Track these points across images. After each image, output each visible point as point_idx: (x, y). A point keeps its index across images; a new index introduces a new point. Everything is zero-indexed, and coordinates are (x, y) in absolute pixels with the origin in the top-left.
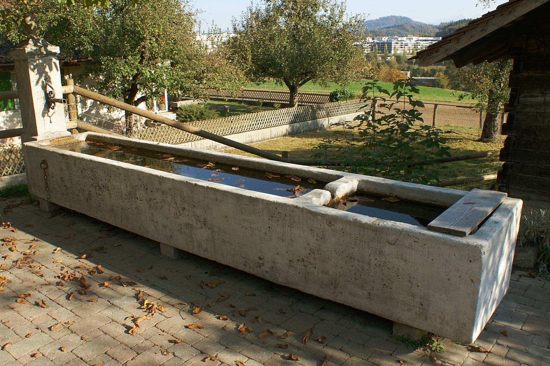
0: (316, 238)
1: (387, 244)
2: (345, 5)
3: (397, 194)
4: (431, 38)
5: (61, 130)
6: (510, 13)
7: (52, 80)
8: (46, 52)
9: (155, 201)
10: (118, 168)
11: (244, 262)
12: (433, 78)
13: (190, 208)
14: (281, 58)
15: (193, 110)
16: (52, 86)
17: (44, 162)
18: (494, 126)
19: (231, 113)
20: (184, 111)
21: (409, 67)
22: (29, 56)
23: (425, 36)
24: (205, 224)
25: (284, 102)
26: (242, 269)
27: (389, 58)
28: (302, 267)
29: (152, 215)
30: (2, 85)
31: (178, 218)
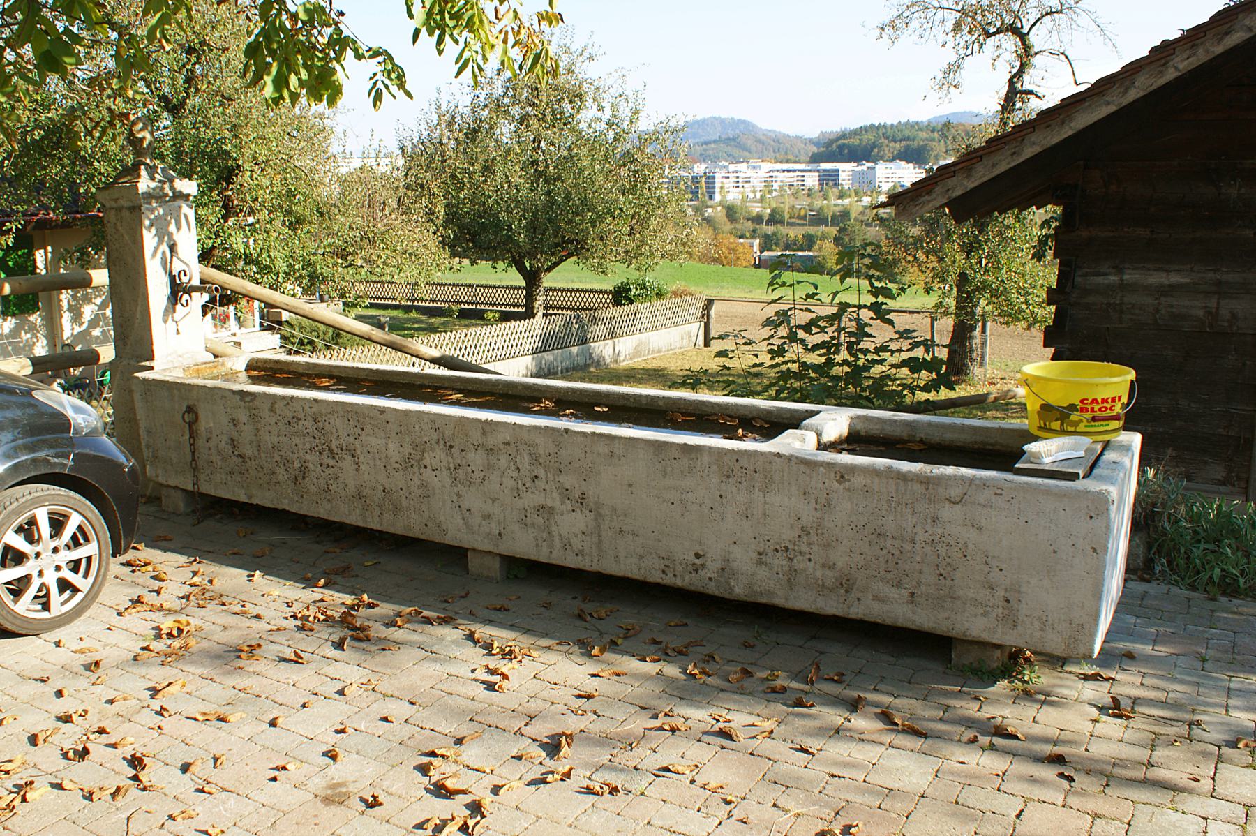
0: (814, 505)
1: (947, 502)
2: (643, 96)
3: (922, 436)
4: (802, 166)
6: (1063, 122)
8: (174, 193)
9: (469, 468)
10: (383, 411)
11: (662, 567)
12: (811, 254)
13: (550, 475)
14: (509, 212)
17: (190, 409)
18: (971, 350)
20: (297, 329)
21: (754, 231)
22: (144, 199)
23: (788, 161)
24: (582, 504)
25: (508, 309)
26: (658, 580)
27: (710, 210)
28: (784, 563)
29: (459, 496)
31: (520, 498)
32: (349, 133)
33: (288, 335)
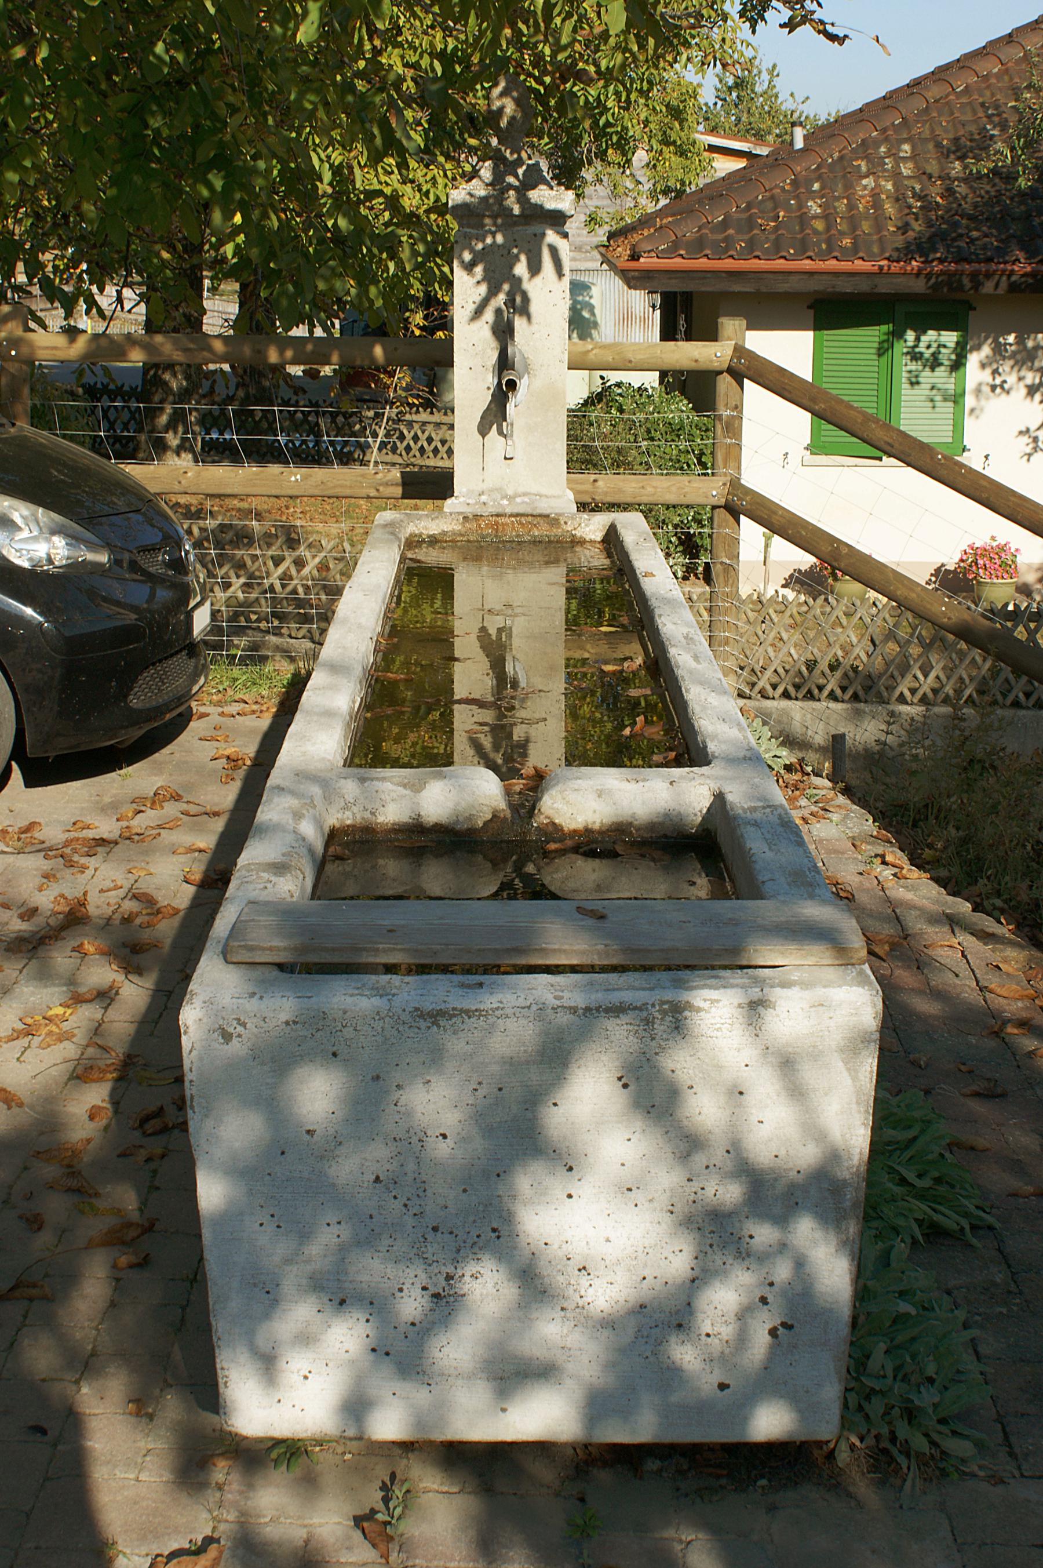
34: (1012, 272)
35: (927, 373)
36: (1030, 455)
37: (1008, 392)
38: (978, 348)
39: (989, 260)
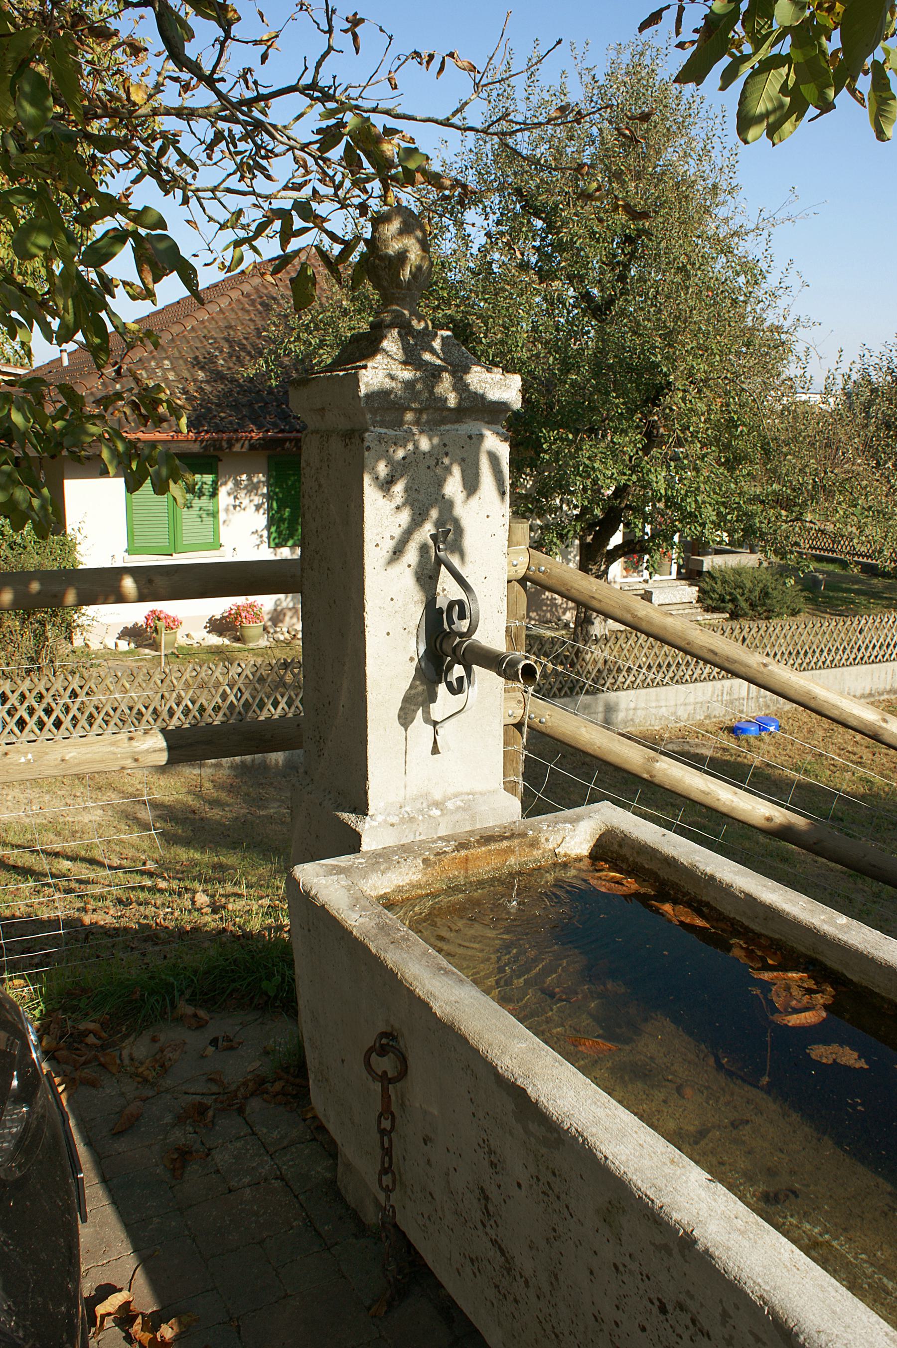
5: (479, 787)
7: (469, 542)
15: (745, 582)
16: (463, 572)
19: (831, 594)
20: (719, 583)
22: (374, 412)
30: (290, 483)
32: (812, 353)
33: (708, 588)
34: (252, 437)
35: (196, 500)
36: (258, 545)
37: (244, 509)
38: (225, 483)
39: (236, 431)
